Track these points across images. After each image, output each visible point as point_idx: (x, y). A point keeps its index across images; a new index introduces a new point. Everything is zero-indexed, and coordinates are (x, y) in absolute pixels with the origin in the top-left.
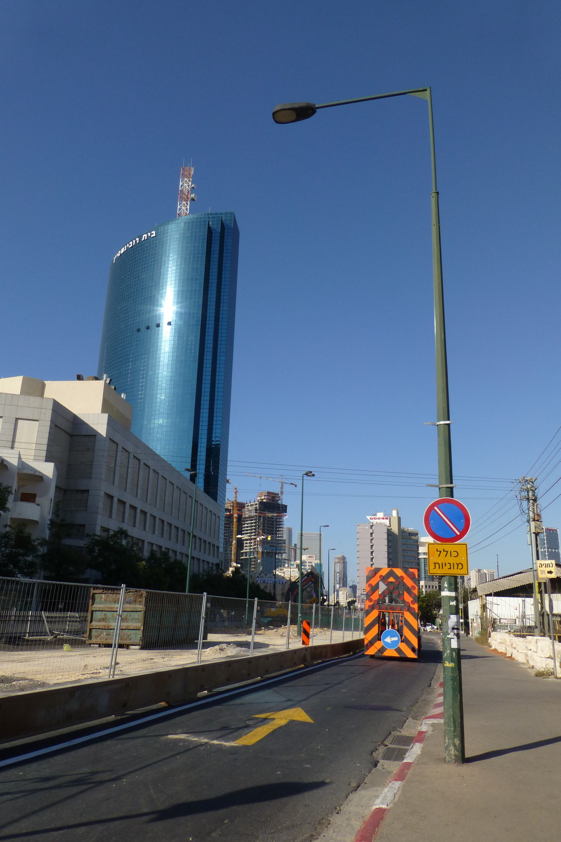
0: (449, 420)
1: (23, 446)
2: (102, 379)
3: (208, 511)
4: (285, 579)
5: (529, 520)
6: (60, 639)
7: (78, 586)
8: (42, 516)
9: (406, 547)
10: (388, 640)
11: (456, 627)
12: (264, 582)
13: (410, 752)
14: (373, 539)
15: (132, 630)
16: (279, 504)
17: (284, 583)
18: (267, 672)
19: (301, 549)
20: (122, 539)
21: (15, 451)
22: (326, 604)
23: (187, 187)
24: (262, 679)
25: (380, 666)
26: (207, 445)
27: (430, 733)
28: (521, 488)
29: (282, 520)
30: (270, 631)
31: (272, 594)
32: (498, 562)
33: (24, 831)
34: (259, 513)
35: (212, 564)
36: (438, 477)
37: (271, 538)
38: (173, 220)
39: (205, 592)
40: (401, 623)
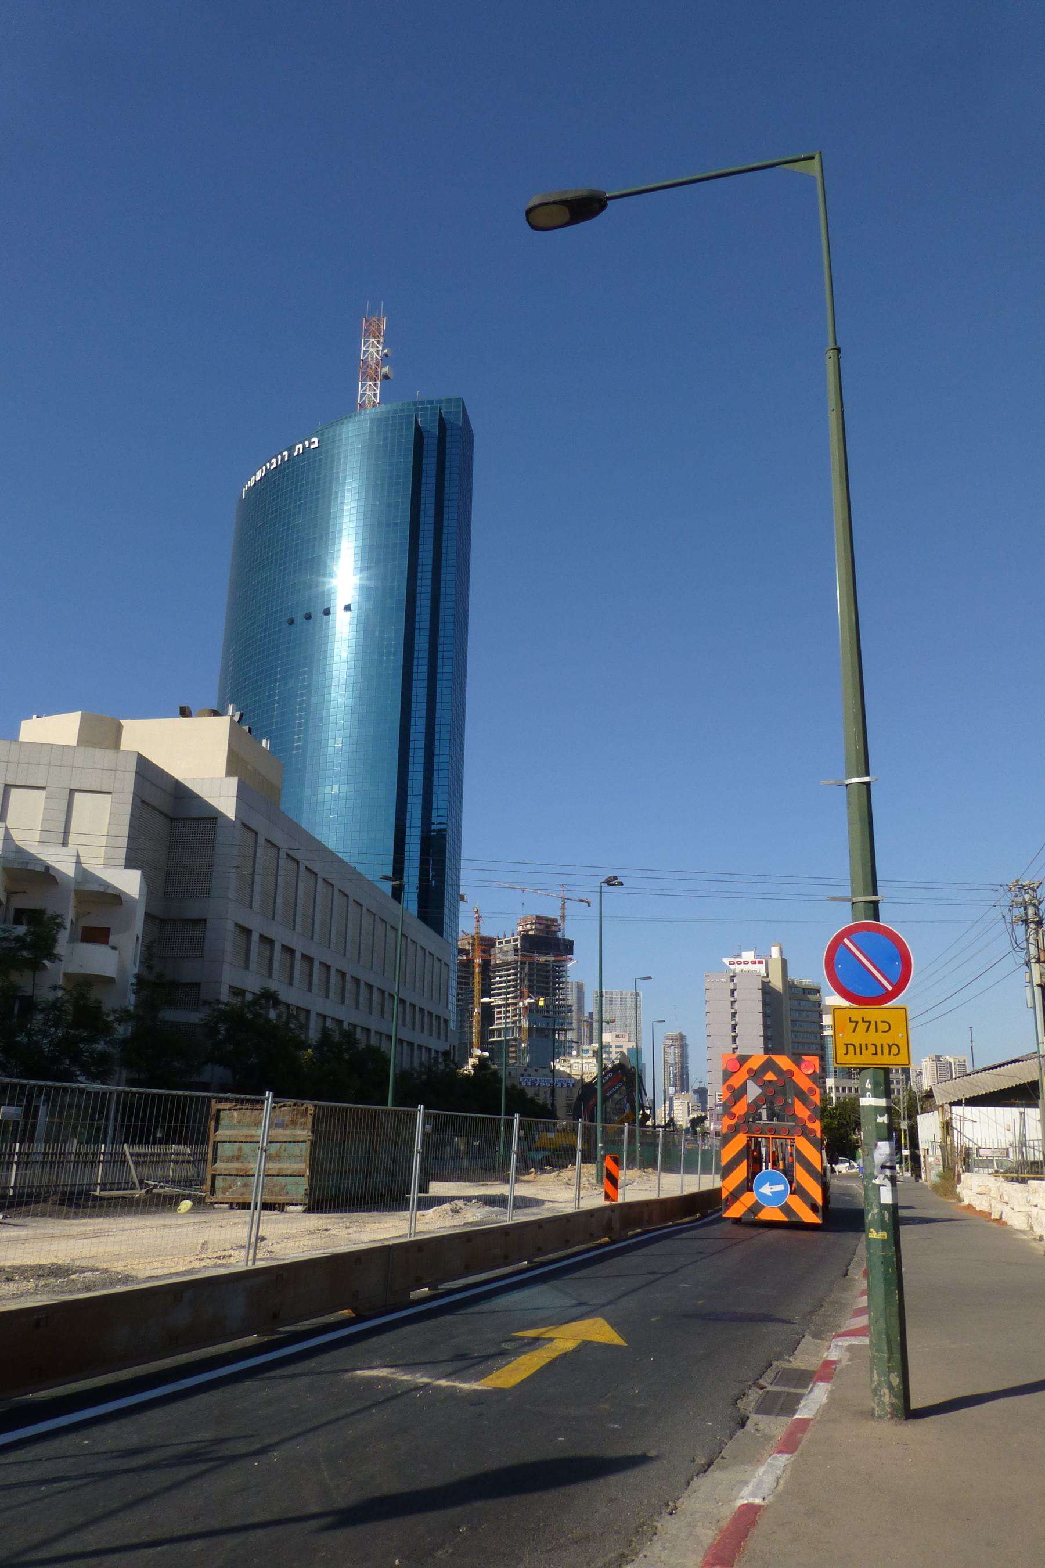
0: (867, 774)
1: (82, 840)
2: (225, 714)
3: (427, 954)
4: (573, 1078)
5: (1029, 961)
6: (159, 1195)
7: (192, 1097)
8: (122, 969)
9: (797, 1015)
10: (766, 1190)
11: (888, 1164)
12: (533, 1084)
13: (807, 1400)
14: (735, 1001)
15: (291, 1176)
16: (558, 939)
17: (571, 1085)
18: (540, 1251)
19: (601, 1021)
20: (269, 1008)
21: (71, 850)
22: (649, 1123)
23: (375, 354)
24: (530, 1265)
25: (752, 1237)
26: (422, 832)
27: (844, 1363)
28: (1013, 902)
29: (564, 968)
30: (546, 1176)
31: (549, 1106)
32: (972, 1041)
33: (91, 1548)
34: (521, 955)
35: (437, 1052)
36: (848, 883)
37: (545, 1003)
38: (350, 417)
39: (421, 1104)
40: (790, 1158)
